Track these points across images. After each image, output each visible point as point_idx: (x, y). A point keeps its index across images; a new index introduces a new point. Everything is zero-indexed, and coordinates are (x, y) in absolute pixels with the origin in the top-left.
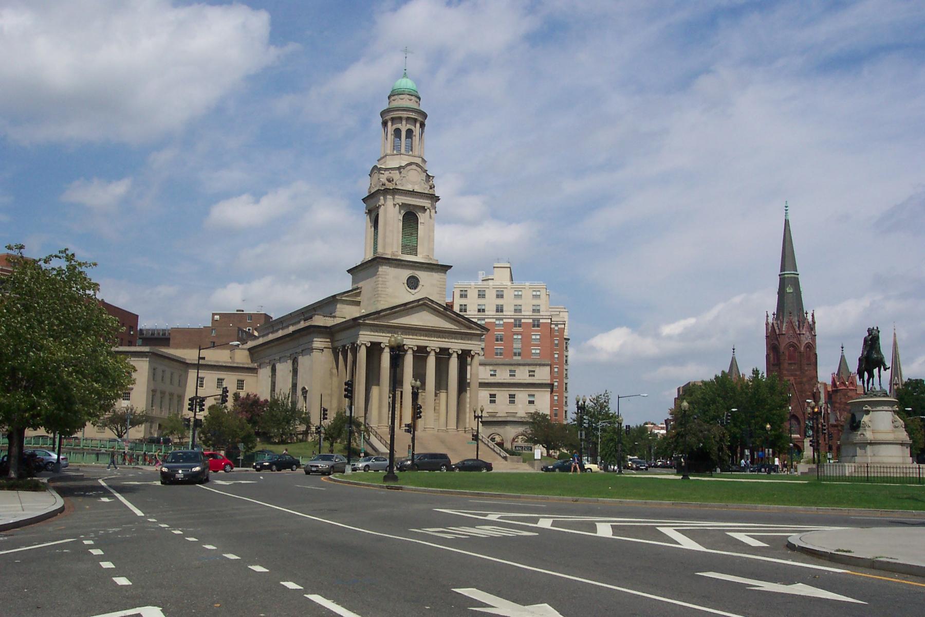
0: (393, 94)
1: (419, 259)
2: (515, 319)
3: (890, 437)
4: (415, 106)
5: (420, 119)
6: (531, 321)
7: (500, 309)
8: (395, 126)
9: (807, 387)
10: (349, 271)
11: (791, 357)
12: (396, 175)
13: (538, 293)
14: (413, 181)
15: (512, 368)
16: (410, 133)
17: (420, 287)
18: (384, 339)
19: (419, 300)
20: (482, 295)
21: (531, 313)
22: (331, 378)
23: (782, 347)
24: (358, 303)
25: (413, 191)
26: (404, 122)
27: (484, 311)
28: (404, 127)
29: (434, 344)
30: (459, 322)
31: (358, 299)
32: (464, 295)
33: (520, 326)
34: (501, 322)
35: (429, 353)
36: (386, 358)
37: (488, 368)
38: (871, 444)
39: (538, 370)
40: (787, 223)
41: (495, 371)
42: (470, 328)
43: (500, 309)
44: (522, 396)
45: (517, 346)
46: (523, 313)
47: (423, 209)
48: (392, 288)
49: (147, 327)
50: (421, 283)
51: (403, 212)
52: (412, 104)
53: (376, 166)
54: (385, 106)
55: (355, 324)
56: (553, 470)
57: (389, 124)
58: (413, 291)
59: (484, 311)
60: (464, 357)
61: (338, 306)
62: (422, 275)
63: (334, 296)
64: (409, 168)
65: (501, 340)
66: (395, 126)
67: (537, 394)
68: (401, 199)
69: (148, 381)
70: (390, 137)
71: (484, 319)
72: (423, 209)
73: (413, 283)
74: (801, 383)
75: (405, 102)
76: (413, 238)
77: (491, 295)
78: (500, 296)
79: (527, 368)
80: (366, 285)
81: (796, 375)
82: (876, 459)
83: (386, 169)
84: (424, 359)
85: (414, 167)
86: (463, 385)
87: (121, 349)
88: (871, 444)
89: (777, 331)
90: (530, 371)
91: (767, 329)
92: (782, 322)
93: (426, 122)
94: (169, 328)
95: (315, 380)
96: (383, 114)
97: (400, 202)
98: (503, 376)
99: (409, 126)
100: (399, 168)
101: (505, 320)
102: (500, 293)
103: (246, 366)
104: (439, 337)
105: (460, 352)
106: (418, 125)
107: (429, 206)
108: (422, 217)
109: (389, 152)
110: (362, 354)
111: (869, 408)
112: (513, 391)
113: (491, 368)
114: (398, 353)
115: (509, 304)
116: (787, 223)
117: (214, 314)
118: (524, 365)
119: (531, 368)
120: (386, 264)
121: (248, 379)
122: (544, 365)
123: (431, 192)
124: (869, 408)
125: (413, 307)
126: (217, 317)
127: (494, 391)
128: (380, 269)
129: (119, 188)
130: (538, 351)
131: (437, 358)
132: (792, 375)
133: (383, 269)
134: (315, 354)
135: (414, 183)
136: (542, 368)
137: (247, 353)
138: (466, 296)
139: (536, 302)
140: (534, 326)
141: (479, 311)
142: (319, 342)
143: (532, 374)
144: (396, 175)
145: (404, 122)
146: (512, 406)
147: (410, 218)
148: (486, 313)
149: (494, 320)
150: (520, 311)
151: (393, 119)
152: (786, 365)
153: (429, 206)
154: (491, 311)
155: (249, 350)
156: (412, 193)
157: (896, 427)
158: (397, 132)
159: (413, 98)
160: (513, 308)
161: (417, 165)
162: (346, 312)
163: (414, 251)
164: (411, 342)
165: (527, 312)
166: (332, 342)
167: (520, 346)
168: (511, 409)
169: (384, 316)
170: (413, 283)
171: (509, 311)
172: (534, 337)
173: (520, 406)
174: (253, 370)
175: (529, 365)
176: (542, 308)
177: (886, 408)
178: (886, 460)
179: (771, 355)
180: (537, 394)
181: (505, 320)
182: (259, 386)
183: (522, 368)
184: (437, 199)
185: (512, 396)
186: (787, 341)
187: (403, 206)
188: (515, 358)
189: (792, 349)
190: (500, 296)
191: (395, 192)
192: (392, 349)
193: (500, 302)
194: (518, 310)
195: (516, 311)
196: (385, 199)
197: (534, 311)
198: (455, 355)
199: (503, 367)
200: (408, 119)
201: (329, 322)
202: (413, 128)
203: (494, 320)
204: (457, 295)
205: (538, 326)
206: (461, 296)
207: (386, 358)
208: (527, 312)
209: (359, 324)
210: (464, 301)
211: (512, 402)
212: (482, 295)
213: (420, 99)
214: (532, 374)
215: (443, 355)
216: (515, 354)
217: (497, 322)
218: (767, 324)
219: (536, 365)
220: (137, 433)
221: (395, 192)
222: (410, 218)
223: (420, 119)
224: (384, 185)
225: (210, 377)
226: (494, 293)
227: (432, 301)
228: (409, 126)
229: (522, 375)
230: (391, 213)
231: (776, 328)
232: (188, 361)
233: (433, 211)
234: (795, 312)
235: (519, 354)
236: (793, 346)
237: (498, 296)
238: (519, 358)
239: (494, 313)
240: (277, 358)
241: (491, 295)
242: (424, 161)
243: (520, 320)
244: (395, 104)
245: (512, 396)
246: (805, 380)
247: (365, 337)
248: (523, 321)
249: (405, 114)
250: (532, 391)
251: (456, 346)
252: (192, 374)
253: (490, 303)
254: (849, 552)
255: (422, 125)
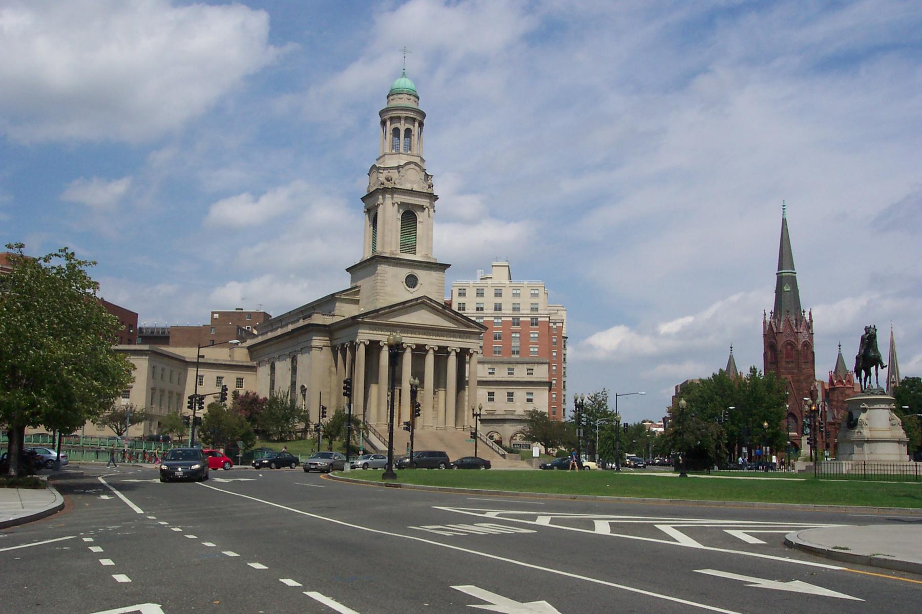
0: (392, 94)
1: (417, 257)
2: (514, 318)
3: (887, 435)
4: (414, 106)
5: (418, 118)
6: (529, 319)
7: (498, 308)
8: (394, 126)
9: (804, 385)
10: (348, 270)
11: (788, 356)
12: (394, 174)
13: (536, 292)
14: (411, 180)
15: (511, 366)
16: (408, 132)
17: (418, 285)
18: (383, 337)
19: (418, 299)
20: (480, 294)
21: (529, 312)
22: (330, 376)
23: (780, 345)
24: (357, 302)
25: (412, 190)
26: (403, 122)
27: (482, 309)
28: (402, 126)
29: (432, 342)
30: (457, 320)
31: (357, 297)
32: (462, 294)
33: (518, 324)
34: (500, 321)
35: (427, 351)
36: (385, 356)
37: (487, 366)
38: (868, 441)
39: (536, 368)
40: (784, 222)
41: (493, 369)
42: (468, 327)
43: (498, 308)
44: (520, 394)
45: (515, 344)
46: (521, 312)
47: (422, 208)
48: (391, 287)
49: (147, 326)
50: (419, 282)
51: (401, 211)
52: (411, 104)
53: (374, 166)
54: (384, 106)
55: (354, 322)
56: (551, 468)
57: (388, 123)
58: (411, 290)
59: (482, 309)
61: (337, 304)
62: (420, 274)
63: (333, 295)
64: (407, 167)
65: (500, 338)
66: (394, 126)
67: (535, 392)
68: (399, 198)
69: (148, 379)
70: (389, 136)
71: (482, 318)
72: (422, 208)
73: (411, 281)
74: (798, 381)
75: (404, 101)
76: (412, 237)
77: (489, 293)
78: (498, 294)
79: (526, 366)
80: (365, 284)
81: (793, 373)
82: (873, 457)
83: (385, 169)
84: (423, 358)
85: (412, 166)
86: (461, 383)
87: (121, 347)
88: (868, 441)
89: (775, 329)
90: (528, 370)
91: (765, 328)
92: (779, 321)
93: (425, 122)
94: (169, 326)
95: (314, 378)
96: (381, 113)
97: (399, 201)
98: (501, 374)
99: (408, 126)
100: (398, 168)
101: (503, 319)
102: (498, 292)
103: (246, 364)
104: (438, 335)
105: (459, 350)
106: (417, 124)
107: (428, 205)
108: (420, 216)
109: (387, 151)
110: (361, 352)
111: (866, 406)
112: (511, 389)
113: (490, 366)
114: (396, 351)
115: (507, 302)
116: (784, 222)
117: (213, 313)
118: (522, 363)
119: (529, 367)
120: (384, 263)
121: (248, 377)
122: (542, 363)
123: (430, 191)
124: (866, 406)
125: (411, 306)
126: (216, 316)
127: (492, 389)
128: (379, 268)
129: (119, 187)
130: (536, 350)
131: (435, 357)
132: (789, 373)
133: (382, 268)
134: (314, 352)
135: (412, 182)
136: (540, 366)
137: (246, 351)
138: (464, 295)
139: (534, 300)
140: (532, 324)
141: (478, 309)
142: (318, 341)
143: (530, 372)
144: (394, 174)
145: (403, 122)
146: (510, 404)
147: (409, 217)
148: (485, 311)
149: (492, 319)
150: (519, 309)
151: (391, 119)
152: (783, 363)
153: (428, 205)
154: (489, 310)
155: (249, 348)
156: (411, 192)
157: (893, 425)
158: (396, 132)
159: (411, 97)
160: (511, 307)
161: (416, 164)
162: (345, 311)
163: (412, 249)
164: (409, 340)
165: (525, 310)
166: (331, 340)
167: (518, 344)
168: (510, 407)
169: (383, 314)
170: (411, 281)
171: (507, 310)
172: (532, 335)
173: (518, 404)
174: (252, 369)
175: (527, 363)
176: (540, 307)
177: (883, 406)
178: (883, 458)
179: (769, 354)
180: (535, 392)
181: (503, 319)
182: (258, 384)
183: (520, 366)
184: (436, 198)
185: (510, 394)
186: (785, 339)
187: (402, 205)
188: (513, 356)
189: (789, 347)
190: (498, 294)
191: (394, 191)
192: (391, 347)
193: (498, 300)
194: (516, 309)
195: (514, 309)
196: (384, 198)
197: (532, 309)
198: (453, 353)
199: (502, 365)
200: (407, 118)
201: (328, 320)
202: (411, 127)
203: (492, 319)
204: (456, 294)
205: (536, 324)
206: (460, 295)
207: (385, 356)
208: (525, 310)
209: (358, 323)
210: (462, 300)
211: (511, 400)
212: (480, 294)
213: (418, 98)
214: (530, 372)
215: (442, 354)
216: (513, 353)
217: (496, 321)
218: (765, 323)
219: (534, 363)
220: (136, 431)
221: (394, 191)
222: (409, 217)
223: (418, 118)
224: (382, 184)
225: (210, 376)
226: (493, 292)
227: (431, 300)
228: (408, 126)
229: (520, 374)
230: (390, 212)
231: (774, 326)
232: (187, 360)
233: (432, 210)
234: (793, 311)
235: (518, 353)
236: (791, 345)
237: (496, 295)
238: (518, 356)
239: (493, 311)
240: (277, 356)
241: (489, 293)
242: (423, 160)
243: (518, 318)
244: (394, 104)
245: (510, 394)
246: (802, 378)
247: (364, 336)
248: (521, 319)
249: (403, 114)
250: (530, 389)
251: (454, 344)
252: (192, 373)
253: (489, 302)
254: (847, 549)
255: (421, 125)
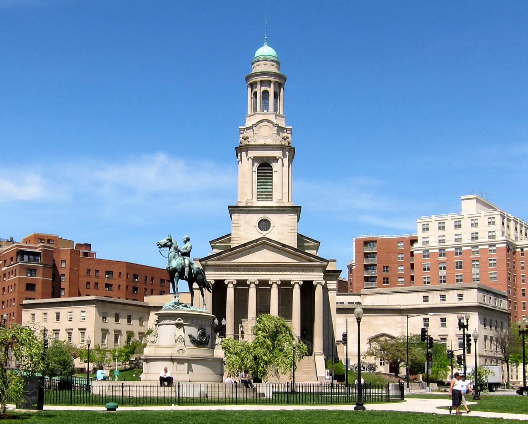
15: (443, 293)
16: (265, 94)
17: (271, 228)
19: (257, 240)
25: (265, 145)
26: (259, 86)
28: (259, 90)
29: (275, 277)
30: (299, 256)
32: (426, 229)
36: (252, 293)
39: (465, 293)
43: (475, 237)
47: (275, 159)
48: (245, 229)
51: (256, 165)
60: (308, 288)
62: (271, 217)
65: (428, 269)
68: (252, 154)
72: (275, 159)
73: (264, 225)
79: (456, 293)
85: (265, 123)
90: (424, 297)
98: (435, 301)
99: (263, 88)
101: (497, 246)
105: (301, 283)
106: (272, 86)
108: (276, 167)
114: (285, 288)
118: (453, 289)
125: (253, 247)
131: (258, 291)
135: (265, 138)
136: (470, 291)
138: (460, 226)
139: (492, 228)
145: (259, 86)
146: (443, 329)
149: (470, 248)
150: (477, 238)
153: (281, 155)
161: (269, 121)
163: (269, 196)
164: (252, 277)
170: (264, 225)
173: (451, 328)
176: (498, 234)
181: (480, 247)
183: (451, 292)
185: (443, 320)
187: (255, 159)
193: (475, 230)
198: (297, 286)
199: (435, 293)
200: (262, 82)
202: (268, 89)
206: (424, 230)
210: (426, 234)
212: (458, 226)
214: (460, 297)
220: (399, 360)
223: (273, 79)
226: (437, 225)
227: (270, 240)
228: (263, 88)
229: (452, 300)
232: (150, 305)
237: (456, 226)
241: (466, 223)
245: (443, 320)
248: (447, 250)
249: (258, 79)
